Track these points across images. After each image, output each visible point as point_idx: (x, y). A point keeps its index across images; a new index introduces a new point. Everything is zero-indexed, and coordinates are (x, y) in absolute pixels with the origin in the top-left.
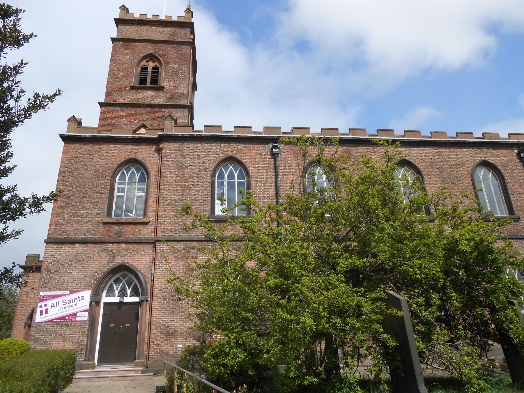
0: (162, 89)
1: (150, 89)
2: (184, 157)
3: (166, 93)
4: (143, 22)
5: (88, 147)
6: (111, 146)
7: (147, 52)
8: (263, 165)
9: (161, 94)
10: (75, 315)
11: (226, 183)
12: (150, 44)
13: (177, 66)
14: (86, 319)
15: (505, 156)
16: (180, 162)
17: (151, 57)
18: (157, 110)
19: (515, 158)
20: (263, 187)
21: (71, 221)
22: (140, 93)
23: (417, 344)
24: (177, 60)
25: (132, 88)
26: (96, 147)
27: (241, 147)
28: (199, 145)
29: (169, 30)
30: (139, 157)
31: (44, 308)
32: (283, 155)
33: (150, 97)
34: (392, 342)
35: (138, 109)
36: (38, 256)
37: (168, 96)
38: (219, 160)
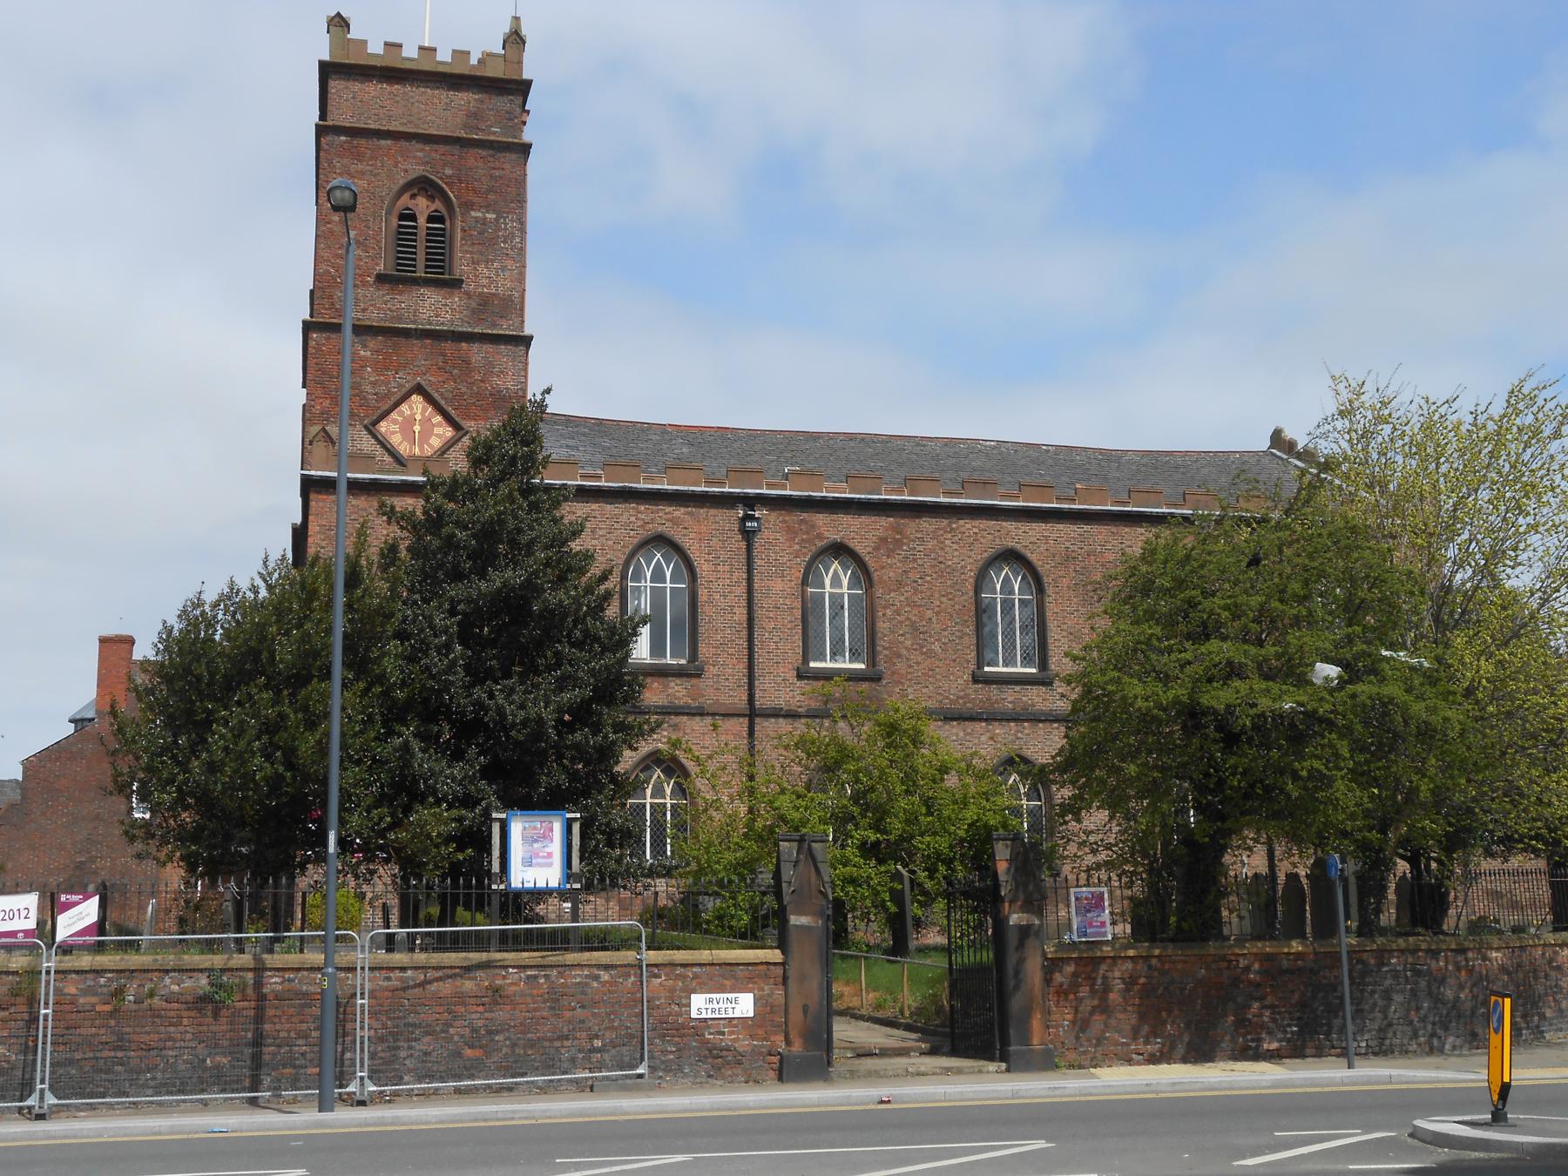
0: (456, 284)
1: (427, 282)
3: (469, 295)
4: (392, 73)
7: (417, 170)
8: (723, 555)
9: (456, 299)
11: (422, 233)
12: (419, 146)
17: (423, 186)
18: (448, 346)
20: (722, 603)
23: (914, 910)
25: (381, 279)
27: (679, 512)
30: (667, 529)
32: (765, 533)
33: (431, 307)
34: (893, 909)
35: (403, 340)
37: (474, 304)
38: (635, 541)
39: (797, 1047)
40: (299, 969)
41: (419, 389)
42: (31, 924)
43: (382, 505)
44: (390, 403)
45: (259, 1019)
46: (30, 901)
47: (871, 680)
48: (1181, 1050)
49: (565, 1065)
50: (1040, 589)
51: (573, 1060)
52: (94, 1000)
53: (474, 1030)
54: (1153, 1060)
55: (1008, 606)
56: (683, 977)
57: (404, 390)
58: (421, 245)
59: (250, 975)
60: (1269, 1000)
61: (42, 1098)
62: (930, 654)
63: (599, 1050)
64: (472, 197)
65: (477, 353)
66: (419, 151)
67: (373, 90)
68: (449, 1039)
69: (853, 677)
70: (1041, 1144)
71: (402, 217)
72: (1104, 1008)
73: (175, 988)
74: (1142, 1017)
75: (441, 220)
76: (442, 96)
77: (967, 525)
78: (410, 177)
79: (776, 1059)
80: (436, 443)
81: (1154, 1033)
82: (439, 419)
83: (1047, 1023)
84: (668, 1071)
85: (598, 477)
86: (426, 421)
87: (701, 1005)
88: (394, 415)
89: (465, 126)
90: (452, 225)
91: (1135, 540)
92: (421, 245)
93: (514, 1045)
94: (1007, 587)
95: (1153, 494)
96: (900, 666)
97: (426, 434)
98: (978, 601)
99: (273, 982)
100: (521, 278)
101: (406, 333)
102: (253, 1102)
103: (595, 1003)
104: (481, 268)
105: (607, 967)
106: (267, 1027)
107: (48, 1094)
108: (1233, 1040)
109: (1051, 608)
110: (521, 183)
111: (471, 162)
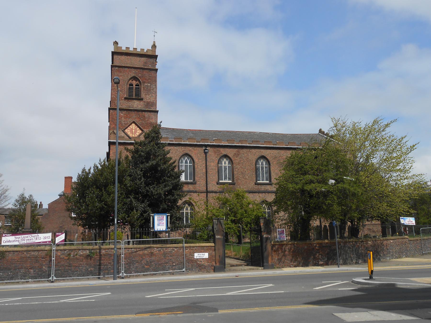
0: (142, 99)
3: (145, 102)
4: (127, 54)
7: (133, 75)
11: (134, 89)
17: (134, 78)
23: (243, 234)
25: (126, 98)
29: (143, 59)
32: (209, 153)
33: (136, 105)
34: (238, 234)
35: (130, 112)
39: (218, 265)
42: (50, 240)
45: (100, 260)
46: (50, 235)
49: (167, 269)
50: (269, 164)
51: (169, 268)
52: (64, 256)
53: (147, 262)
54: (295, 266)
55: (262, 168)
56: (193, 249)
58: (134, 91)
59: (98, 250)
61: (53, 278)
62: (246, 179)
65: (147, 114)
66: (134, 71)
67: (123, 57)
69: (230, 184)
70: (271, 285)
71: (130, 85)
72: (284, 255)
73: (82, 253)
74: (293, 257)
75: (138, 86)
76: (138, 59)
77: (253, 151)
80: (138, 134)
81: (295, 261)
82: (138, 129)
83: (273, 258)
84: (190, 270)
85: (173, 141)
86: (135, 129)
87: (197, 256)
88: (129, 128)
89: (144, 65)
91: (288, 153)
92: (134, 91)
93: (156, 265)
95: (294, 143)
96: (239, 181)
97: (136, 132)
98: (256, 167)
99: (103, 252)
100: (156, 98)
101: (131, 110)
102: (99, 278)
105: (176, 248)
109: (272, 168)
110: (156, 77)
111: (145, 73)
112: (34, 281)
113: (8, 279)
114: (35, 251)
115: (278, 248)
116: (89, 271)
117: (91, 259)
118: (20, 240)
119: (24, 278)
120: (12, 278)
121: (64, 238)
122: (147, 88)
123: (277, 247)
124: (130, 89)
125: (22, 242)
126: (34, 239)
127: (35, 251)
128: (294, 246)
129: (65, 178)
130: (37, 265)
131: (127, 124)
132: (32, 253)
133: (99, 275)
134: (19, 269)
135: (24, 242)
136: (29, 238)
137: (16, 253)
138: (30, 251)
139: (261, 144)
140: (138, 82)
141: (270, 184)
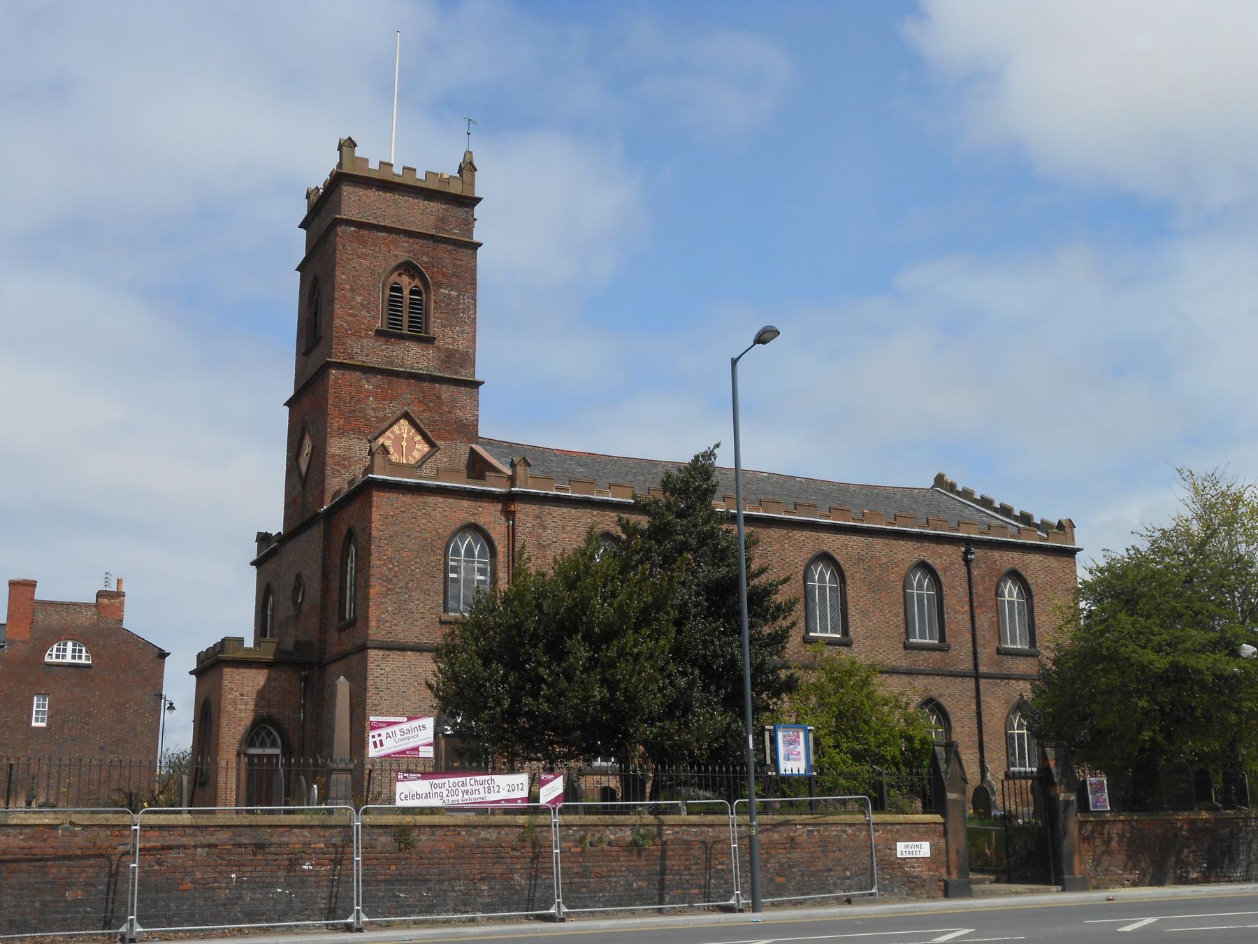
0: (430, 341)
2: (545, 528)
3: (438, 348)
5: (407, 499)
6: (441, 500)
7: (404, 257)
10: (417, 749)
11: (406, 302)
13: (454, 293)
14: (431, 755)
15: (948, 555)
16: (539, 535)
17: (408, 268)
19: (960, 559)
21: (397, 617)
22: (392, 344)
24: (454, 279)
25: (379, 333)
26: (419, 499)
28: (565, 510)
29: (435, 207)
31: (377, 739)
33: (413, 356)
36: (241, 640)
39: (954, 877)
40: (682, 825)
41: (406, 416)
42: (525, 794)
43: (620, 519)
44: (387, 424)
45: (663, 857)
46: (523, 779)
47: (942, 650)
48: (1148, 878)
50: (843, 581)
51: (835, 884)
52: (570, 844)
53: (781, 865)
54: (1135, 884)
55: (822, 589)
57: (396, 416)
58: (406, 310)
60: (1193, 847)
63: (848, 878)
64: (440, 278)
65: (446, 392)
66: (405, 242)
67: (373, 195)
68: (767, 871)
69: (831, 642)
72: (1108, 852)
74: (1129, 858)
76: (421, 204)
77: (798, 534)
78: (399, 261)
79: (942, 884)
80: (417, 455)
82: (419, 438)
83: (1081, 863)
84: (888, 891)
85: (567, 490)
87: (904, 849)
88: (388, 433)
89: (436, 227)
90: (428, 298)
91: (587, 518)
92: (406, 310)
93: (803, 875)
94: (822, 576)
95: (910, 519)
97: (411, 448)
98: (805, 586)
99: (668, 833)
100: (473, 340)
101: (397, 374)
102: (660, 911)
103: (846, 848)
104: (447, 330)
106: (668, 862)
107: (362, 915)
108: (1175, 872)
109: (850, 594)
110: (473, 271)
111: (441, 254)
112: (489, 918)
113: (420, 913)
114: (489, 826)
115: (1093, 831)
116: (633, 890)
117: (639, 855)
118: (445, 793)
119: (463, 908)
120: (430, 909)
121: (560, 790)
122: (447, 305)
123: (1089, 828)
124: (394, 304)
125: (451, 798)
126: (482, 790)
127: (489, 826)
128: (1132, 827)
129: (13, 584)
130: (499, 869)
131: (385, 418)
132: (483, 834)
133: (661, 902)
134: (449, 880)
135: (455, 798)
136: (469, 787)
137: (439, 832)
138: (475, 827)
139: (821, 516)
140: (417, 282)
141: (1031, 654)
